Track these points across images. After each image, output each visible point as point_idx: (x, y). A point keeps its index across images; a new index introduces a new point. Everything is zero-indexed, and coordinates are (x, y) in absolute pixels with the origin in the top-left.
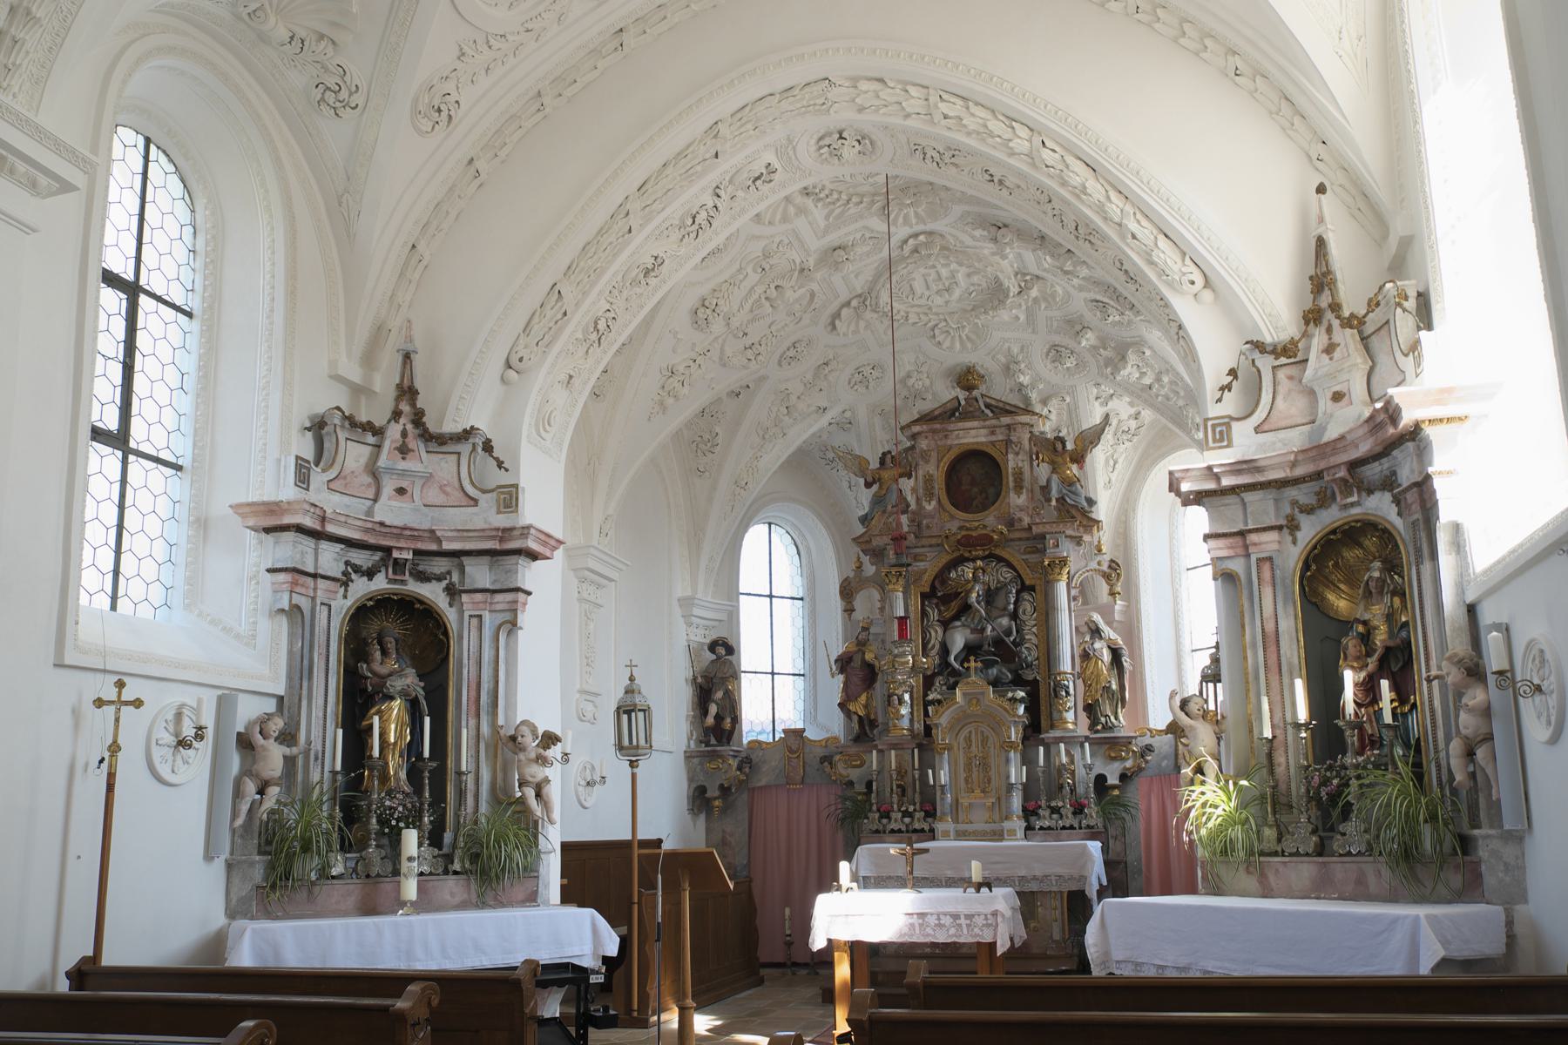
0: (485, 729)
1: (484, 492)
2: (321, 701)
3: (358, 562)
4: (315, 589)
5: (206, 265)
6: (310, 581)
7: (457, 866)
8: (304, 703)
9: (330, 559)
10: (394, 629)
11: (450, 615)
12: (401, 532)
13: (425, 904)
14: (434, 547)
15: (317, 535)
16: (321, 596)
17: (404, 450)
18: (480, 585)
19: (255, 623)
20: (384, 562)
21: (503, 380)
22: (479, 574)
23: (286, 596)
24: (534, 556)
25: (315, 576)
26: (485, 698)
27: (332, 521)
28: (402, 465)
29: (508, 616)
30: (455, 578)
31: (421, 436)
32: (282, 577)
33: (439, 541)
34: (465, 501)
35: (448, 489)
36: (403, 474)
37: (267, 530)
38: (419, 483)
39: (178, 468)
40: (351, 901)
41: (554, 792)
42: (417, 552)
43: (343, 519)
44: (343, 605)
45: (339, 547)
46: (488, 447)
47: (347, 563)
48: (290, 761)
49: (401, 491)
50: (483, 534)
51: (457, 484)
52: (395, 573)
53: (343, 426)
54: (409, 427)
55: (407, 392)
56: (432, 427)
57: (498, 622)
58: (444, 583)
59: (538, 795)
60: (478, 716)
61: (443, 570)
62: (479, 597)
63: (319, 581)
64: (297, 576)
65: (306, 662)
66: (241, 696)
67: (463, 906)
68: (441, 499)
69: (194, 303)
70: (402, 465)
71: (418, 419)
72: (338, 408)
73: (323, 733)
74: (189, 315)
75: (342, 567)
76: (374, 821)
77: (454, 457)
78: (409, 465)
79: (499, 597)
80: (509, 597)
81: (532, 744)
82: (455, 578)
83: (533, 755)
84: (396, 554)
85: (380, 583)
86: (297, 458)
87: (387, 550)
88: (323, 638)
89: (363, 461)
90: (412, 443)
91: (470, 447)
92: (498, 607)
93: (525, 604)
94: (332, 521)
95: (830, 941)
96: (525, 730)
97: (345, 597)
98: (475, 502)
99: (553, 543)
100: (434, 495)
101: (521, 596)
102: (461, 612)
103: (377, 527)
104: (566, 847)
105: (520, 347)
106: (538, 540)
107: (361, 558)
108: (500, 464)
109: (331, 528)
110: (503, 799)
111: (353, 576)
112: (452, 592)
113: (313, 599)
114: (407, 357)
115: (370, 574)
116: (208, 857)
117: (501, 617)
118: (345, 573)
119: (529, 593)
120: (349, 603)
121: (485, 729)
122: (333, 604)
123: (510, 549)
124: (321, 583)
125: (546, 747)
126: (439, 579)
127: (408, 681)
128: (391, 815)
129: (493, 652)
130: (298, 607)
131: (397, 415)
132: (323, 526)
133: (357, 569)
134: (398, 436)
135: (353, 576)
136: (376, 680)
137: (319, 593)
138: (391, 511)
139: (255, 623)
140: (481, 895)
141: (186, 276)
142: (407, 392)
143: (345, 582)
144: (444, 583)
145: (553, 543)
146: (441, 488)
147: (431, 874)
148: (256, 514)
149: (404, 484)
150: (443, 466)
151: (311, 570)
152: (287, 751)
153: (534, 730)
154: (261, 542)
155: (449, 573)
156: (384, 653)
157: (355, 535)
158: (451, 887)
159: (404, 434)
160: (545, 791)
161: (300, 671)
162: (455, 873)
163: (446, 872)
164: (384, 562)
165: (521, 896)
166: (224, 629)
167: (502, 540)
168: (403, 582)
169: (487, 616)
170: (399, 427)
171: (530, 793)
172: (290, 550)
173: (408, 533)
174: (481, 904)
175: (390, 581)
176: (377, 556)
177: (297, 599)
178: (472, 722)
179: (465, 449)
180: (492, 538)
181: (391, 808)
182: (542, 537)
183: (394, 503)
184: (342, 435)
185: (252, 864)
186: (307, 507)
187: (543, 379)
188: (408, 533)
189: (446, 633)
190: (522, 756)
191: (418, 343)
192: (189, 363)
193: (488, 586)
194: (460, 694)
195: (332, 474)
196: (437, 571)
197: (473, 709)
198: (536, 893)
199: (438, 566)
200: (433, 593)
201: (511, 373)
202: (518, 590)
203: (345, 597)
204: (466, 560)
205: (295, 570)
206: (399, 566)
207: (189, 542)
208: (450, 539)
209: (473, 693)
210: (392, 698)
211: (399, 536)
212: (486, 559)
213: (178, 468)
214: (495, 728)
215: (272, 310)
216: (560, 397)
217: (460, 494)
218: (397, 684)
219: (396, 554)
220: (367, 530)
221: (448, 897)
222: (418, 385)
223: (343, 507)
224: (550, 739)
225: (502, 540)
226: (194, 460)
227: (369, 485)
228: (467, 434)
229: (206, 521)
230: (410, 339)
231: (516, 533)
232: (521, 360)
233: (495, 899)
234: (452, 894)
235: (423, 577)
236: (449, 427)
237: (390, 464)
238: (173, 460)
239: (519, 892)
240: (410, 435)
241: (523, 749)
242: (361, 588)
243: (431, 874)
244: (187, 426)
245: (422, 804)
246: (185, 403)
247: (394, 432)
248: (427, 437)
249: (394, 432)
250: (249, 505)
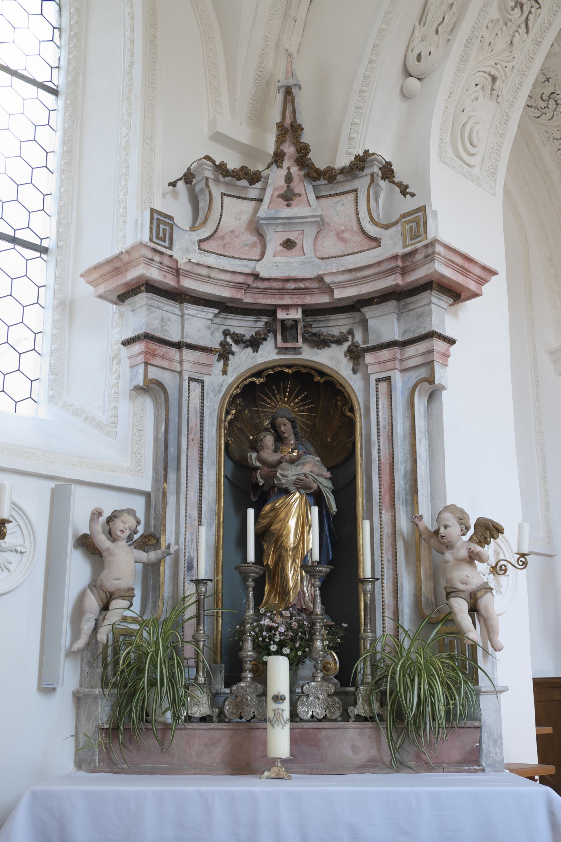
0: (403, 523)
1: (386, 227)
2: (193, 497)
3: (238, 331)
4: (181, 362)
5: (70, 39)
6: (173, 353)
7: (360, 709)
8: (171, 500)
9: (200, 326)
10: (287, 409)
11: (354, 383)
12: (284, 285)
13: (308, 756)
14: (324, 299)
15: (178, 296)
16: (189, 369)
17: (288, 197)
18: (386, 339)
19: (116, 408)
20: (270, 329)
21: (405, 95)
22: (385, 324)
23: (141, 370)
24: (455, 294)
25: (178, 346)
26: (400, 483)
27: (189, 274)
28: (287, 212)
29: (423, 373)
30: (358, 337)
31: (307, 176)
32: (138, 347)
33: (329, 290)
34: (366, 244)
35: (346, 235)
36: (289, 222)
37: (122, 298)
38: (310, 232)
39: (44, 250)
40: (217, 753)
41: (497, 604)
42: (308, 311)
43: (204, 272)
44: (221, 381)
45: (211, 312)
46: (387, 172)
47: (226, 333)
48: (151, 572)
49: (289, 244)
50: (381, 269)
51: (355, 227)
52: (285, 340)
53: (216, 180)
54: (295, 170)
55: (290, 130)
56: (320, 161)
57: (411, 384)
58: (346, 345)
59: (474, 609)
60: (393, 506)
61: (344, 329)
62: (385, 354)
63: (185, 351)
64: (154, 346)
65: (172, 450)
66: (73, 486)
67: (370, 766)
68: (339, 248)
69: (58, 80)
70: (287, 212)
71: (303, 158)
72: (207, 158)
73: (196, 540)
74: (55, 92)
75: (220, 337)
76: (249, 645)
77: (351, 196)
78: (297, 210)
79: (411, 350)
80: (422, 347)
81: (463, 541)
82: (358, 337)
83: (463, 553)
84: (281, 315)
85: (268, 354)
86: (152, 211)
87: (271, 311)
88: (195, 421)
89: (245, 218)
90: (298, 186)
91: (368, 179)
92: (411, 363)
93: (446, 356)
94: (189, 274)
95: (366, 152)
96: (449, 518)
97: (225, 372)
98: (377, 241)
99: (477, 271)
100: (330, 246)
101: (438, 345)
102: (366, 378)
103: (250, 280)
104: (542, 686)
105: (417, 40)
106: (450, 263)
107: (244, 326)
108: (404, 190)
109: (188, 283)
110: (435, 616)
111: (235, 348)
112: (355, 355)
113: (180, 373)
114: (288, 92)
115: (254, 343)
116: (47, 689)
117: (415, 376)
118: (223, 344)
119: (452, 342)
120: (230, 378)
121: (403, 523)
122: (206, 379)
123: (421, 283)
124: (189, 355)
125: (483, 542)
126: (339, 341)
127: (307, 469)
128: (271, 638)
129: (408, 423)
130: (160, 384)
131: (278, 158)
132: (178, 281)
133: (238, 340)
134: (282, 182)
135: (235, 348)
136: (266, 470)
137: (186, 366)
138: (275, 264)
139: (116, 408)
140: (395, 749)
141: (51, 53)
142: (290, 130)
143: (224, 354)
144: (346, 345)
145: (477, 271)
146: (338, 235)
147: (325, 719)
148: (104, 278)
149: (293, 236)
150: (339, 211)
151: (176, 338)
152: (143, 556)
153: (462, 518)
154: (122, 316)
155: (351, 332)
156: (279, 439)
157: (226, 293)
158: (352, 739)
159: (289, 178)
160: (484, 601)
161: (166, 462)
162: (358, 718)
163: (345, 717)
164: (270, 329)
165: (456, 755)
166: (86, 419)
167: (404, 272)
168: (296, 350)
169: (398, 378)
170: (283, 172)
171: (460, 607)
172: (145, 314)
173: (291, 285)
174: (397, 765)
175: (281, 350)
176: (261, 323)
177: (154, 373)
178: (387, 516)
179: (362, 183)
180: (391, 271)
181: (270, 629)
182: (458, 260)
183: (280, 259)
184: (216, 191)
185: (95, 698)
186: (150, 254)
187: (451, 79)
188: (291, 285)
189: (352, 410)
190: (448, 556)
191: (304, 75)
192: (52, 140)
193: (397, 337)
194: (370, 481)
195: (205, 232)
196: (336, 332)
197: (387, 497)
198: (479, 750)
199: (338, 325)
200: (332, 360)
201: (412, 81)
202: (432, 335)
203: (225, 372)
204: (368, 312)
205: (147, 337)
206: (288, 329)
207: (54, 327)
208: (342, 285)
209: (386, 478)
210: (287, 492)
211: (281, 292)
212: (391, 305)
213: (44, 250)
214: (415, 519)
215: (131, 66)
216: (484, 111)
217: (359, 238)
218: (288, 474)
219: (281, 315)
220: (238, 286)
221: (349, 753)
222: (302, 120)
223: (213, 267)
224: (488, 530)
225: (404, 272)
226: (58, 240)
227: (254, 245)
228: (361, 162)
229: (72, 303)
230: (291, 73)
231: (419, 257)
232: (419, 57)
233: (418, 757)
234: (354, 748)
235: (320, 342)
236: (343, 160)
237: (272, 213)
238: (37, 241)
239: (453, 746)
240: (296, 178)
241: (449, 546)
242: (244, 361)
243: (325, 719)
244: (51, 205)
245: (313, 624)
246: (48, 182)
247: (276, 178)
248: (313, 174)
249: (276, 178)
250: (96, 268)
